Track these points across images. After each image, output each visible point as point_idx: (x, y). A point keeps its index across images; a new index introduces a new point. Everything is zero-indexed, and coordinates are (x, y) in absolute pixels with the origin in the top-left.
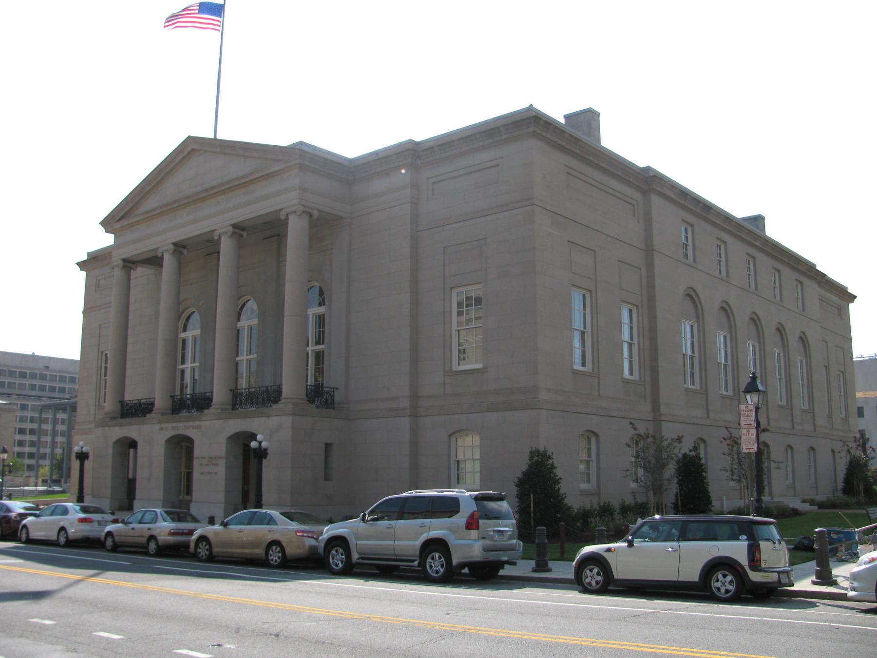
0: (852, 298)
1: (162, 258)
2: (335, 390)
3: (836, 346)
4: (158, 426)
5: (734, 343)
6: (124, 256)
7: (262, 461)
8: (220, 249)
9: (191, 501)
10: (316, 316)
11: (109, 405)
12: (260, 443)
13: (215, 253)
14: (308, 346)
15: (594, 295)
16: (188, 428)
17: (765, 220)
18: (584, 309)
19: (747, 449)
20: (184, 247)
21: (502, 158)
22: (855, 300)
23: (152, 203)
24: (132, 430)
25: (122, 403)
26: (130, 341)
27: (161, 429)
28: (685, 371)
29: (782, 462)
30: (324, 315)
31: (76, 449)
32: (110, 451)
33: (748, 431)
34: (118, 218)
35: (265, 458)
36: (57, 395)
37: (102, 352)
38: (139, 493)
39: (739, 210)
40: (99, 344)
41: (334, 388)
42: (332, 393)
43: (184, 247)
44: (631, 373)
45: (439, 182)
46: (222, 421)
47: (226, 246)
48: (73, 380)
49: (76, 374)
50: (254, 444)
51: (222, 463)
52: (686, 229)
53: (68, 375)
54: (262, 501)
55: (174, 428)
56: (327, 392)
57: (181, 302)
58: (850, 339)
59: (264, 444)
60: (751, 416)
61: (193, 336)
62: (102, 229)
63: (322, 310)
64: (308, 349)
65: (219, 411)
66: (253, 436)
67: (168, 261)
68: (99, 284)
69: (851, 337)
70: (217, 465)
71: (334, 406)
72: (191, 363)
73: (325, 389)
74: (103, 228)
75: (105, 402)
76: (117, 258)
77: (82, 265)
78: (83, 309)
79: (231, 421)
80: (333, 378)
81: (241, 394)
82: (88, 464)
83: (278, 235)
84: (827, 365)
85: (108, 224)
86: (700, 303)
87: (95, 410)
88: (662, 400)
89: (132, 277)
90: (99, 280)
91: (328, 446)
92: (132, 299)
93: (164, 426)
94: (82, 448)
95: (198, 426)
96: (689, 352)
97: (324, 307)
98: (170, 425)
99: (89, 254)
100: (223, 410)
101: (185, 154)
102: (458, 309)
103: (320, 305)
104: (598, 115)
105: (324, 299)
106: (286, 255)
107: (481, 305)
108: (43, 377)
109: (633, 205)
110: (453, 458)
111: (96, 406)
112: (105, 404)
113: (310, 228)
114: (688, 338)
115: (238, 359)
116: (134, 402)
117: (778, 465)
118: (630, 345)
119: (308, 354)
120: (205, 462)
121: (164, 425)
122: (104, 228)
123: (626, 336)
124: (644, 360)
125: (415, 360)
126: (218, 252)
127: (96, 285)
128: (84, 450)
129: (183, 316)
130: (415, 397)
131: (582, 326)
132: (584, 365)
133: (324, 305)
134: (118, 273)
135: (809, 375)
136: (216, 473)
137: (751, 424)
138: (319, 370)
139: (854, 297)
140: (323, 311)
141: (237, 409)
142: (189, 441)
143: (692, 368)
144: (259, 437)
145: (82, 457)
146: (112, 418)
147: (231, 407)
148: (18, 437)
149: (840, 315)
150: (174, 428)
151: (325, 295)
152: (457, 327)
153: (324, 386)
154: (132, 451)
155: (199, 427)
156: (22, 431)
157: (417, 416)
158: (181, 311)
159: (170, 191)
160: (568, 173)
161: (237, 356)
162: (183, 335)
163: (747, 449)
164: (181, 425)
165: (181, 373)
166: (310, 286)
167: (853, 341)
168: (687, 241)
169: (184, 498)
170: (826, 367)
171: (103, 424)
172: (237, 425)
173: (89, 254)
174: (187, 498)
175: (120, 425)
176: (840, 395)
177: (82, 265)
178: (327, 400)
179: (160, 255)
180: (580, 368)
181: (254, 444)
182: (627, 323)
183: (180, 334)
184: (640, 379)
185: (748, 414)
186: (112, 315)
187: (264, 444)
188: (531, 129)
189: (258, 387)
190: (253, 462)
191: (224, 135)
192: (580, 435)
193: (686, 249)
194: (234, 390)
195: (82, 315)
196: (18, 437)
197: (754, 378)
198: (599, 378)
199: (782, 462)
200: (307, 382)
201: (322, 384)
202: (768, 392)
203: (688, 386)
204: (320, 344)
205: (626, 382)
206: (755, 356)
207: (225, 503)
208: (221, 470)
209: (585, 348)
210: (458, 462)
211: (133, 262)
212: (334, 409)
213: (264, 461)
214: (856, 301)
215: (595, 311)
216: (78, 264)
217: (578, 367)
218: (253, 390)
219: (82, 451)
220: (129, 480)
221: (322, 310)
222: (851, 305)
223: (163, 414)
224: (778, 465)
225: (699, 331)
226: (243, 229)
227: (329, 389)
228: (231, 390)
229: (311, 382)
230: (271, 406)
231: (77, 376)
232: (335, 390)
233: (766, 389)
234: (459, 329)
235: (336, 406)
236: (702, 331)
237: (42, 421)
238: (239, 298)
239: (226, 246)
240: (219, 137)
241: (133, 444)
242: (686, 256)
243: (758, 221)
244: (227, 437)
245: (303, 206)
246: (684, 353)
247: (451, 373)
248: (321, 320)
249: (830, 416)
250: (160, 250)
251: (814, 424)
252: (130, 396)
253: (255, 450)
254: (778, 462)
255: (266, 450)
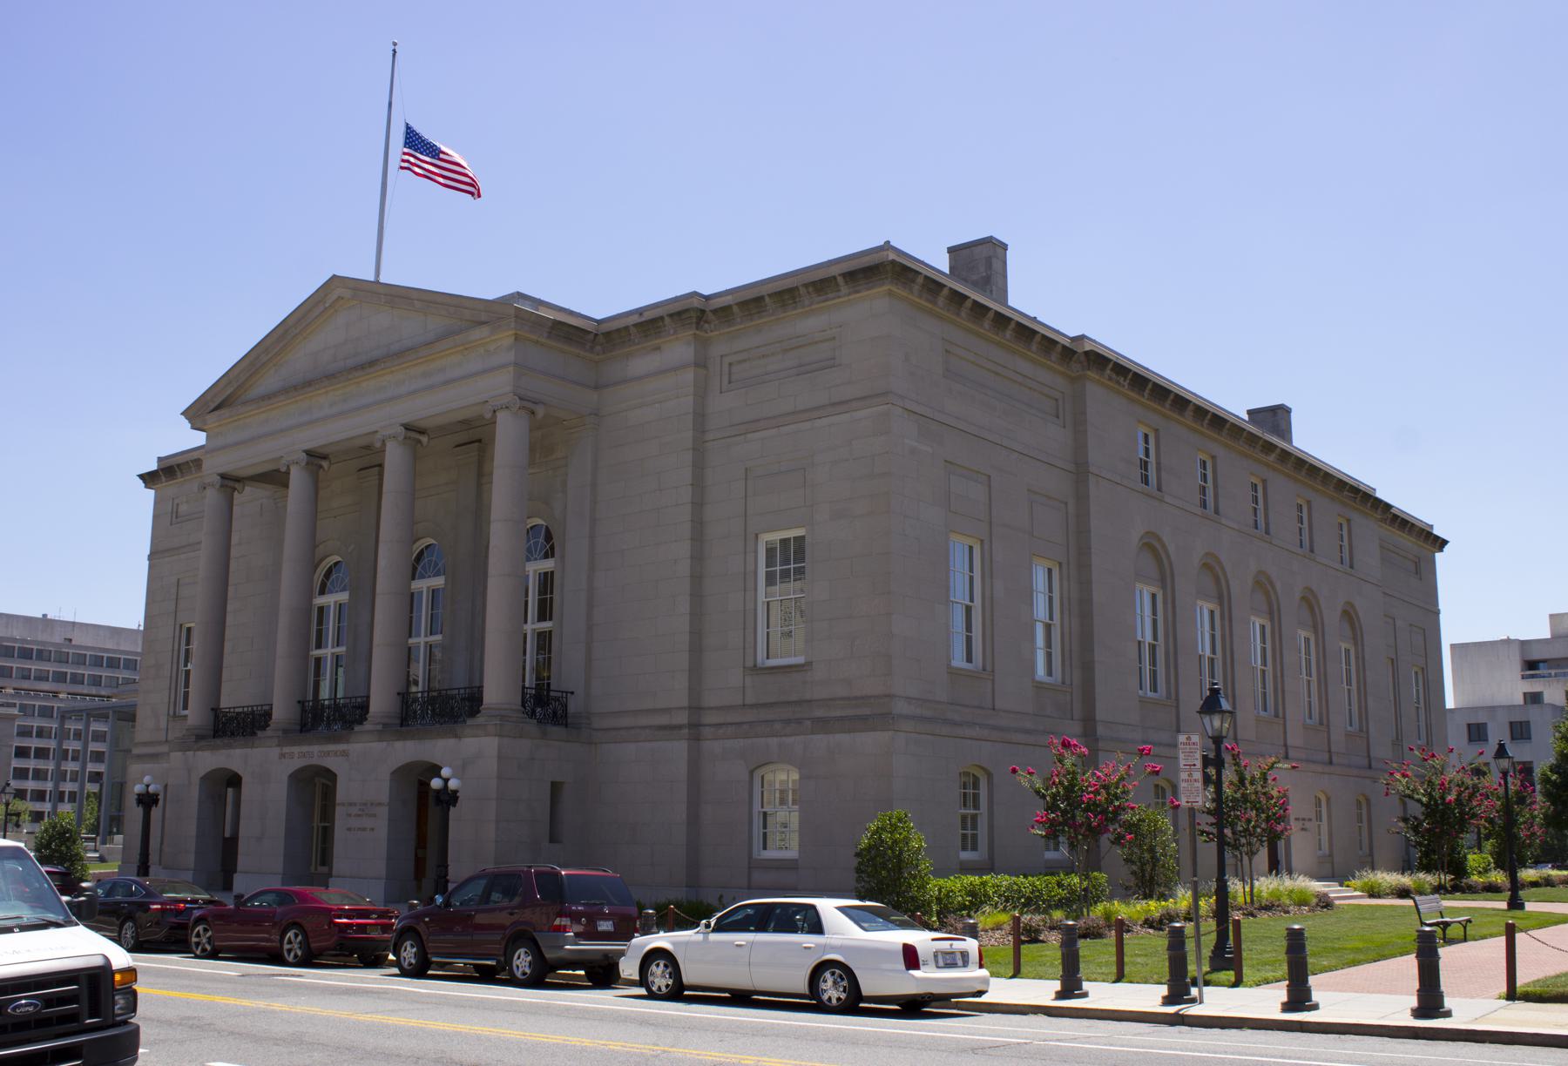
0: (1441, 544)
1: (287, 473)
2: (569, 695)
3: (1411, 625)
4: (275, 752)
5: (1227, 623)
6: (222, 470)
7: (449, 809)
8: (383, 459)
9: (330, 875)
10: (540, 574)
11: (195, 715)
12: (446, 781)
13: (375, 466)
14: (526, 622)
15: (986, 547)
16: (328, 754)
17: (1292, 414)
18: (971, 570)
19: (1188, 802)
20: (324, 457)
21: (841, 326)
22: (1446, 547)
23: (269, 381)
24: (233, 757)
25: (216, 711)
26: (230, 608)
27: (283, 756)
28: (1140, 668)
29: (1310, 820)
30: (552, 573)
31: (138, 788)
32: (195, 792)
33: (1190, 775)
34: (213, 406)
35: (455, 806)
36: (85, 689)
37: (181, 625)
38: (242, 861)
39: (1237, 403)
40: (176, 611)
41: (567, 693)
42: (564, 699)
43: (324, 457)
44: (1050, 673)
45: (740, 362)
46: (385, 744)
47: (395, 458)
48: (131, 665)
49: (136, 654)
50: (436, 783)
51: (384, 812)
52: (1146, 436)
53: (105, 655)
54: (447, 875)
55: (303, 755)
56: (556, 699)
57: (318, 546)
58: (1436, 613)
59: (453, 784)
60: (1195, 752)
61: (336, 602)
62: (186, 424)
63: (548, 565)
64: (525, 627)
65: (380, 727)
66: (435, 770)
67: (297, 478)
68: (177, 512)
69: (1439, 610)
70: (374, 815)
71: (567, 721)
72: (333, 647)
73: (552, 694)
74: (187, 421)
75: (185, 707)
76: (213, 467)
77: (149, 479)
78: (148, 553)
79: (399, 745)
80: (567, 675)
81: (415, 700)
82: (156, 812)
83: (479, 441)
84: (1394, 657)
85: (196, 414)
86: (1168, 556)
87: (744, 676)
88: (1100, 714)
89: (235, 502)
90: (178, 505)
91: (556, 788)
92: (235, 539)
93: (287, 751)
94: (148, 786)
95: (344, 751)
96: (1149, 638)
97: (553, 559)
98: (296, 750)
99: (160, 459)
100: (385, 725)
101: (327, 305)
102: (767, 567)
103: (546, 556)
104: (1004, 247)
105: (552, 548)
106: (491, 474)
107: (804, 562)
108: (63, 659)
109: (1057, 400)
110: (757, 807)
111: (168, 714)
112: (186, 712)
113: (531, 431)
114: (1146, 614)
115: (411, 641)
116: (237, 710)
117: (1303, 824)
118: (1048, 628)
119: (525, 635)
120: (354, 810)
121: (286, 750)
122: (190, 422)
123: (1041, 610)
124: (1071, 651)
125: (697, 648)
126: (381, 466)
127: (172, 512)
128: (151, 789)
129: (319, 570)
130: (696, 709)
131: (967, 597)
132: (969, 660)
133: (553, 556)
134: (212, 497)
135: (1323, 684)
136: (372, 829)
137: (1194, 765)
138: (544, 665)
139: (1444, 542)
140: (549, 566)
141: (408, 725)
142: (330, 776)
143: (1153, 662)
144: (445, 772)
145: (148, 801)
146: (200, 738)
147: (398, 721)
148: (17, 763)
149: (1417, 572)
150: (303, 755)
151: (554, 540)
152: (766, 597)
153: (552, 688)
154: (230, 790)
155: (345, 754)
156: (22, 753)
157: (699, 740)
158: (316, 562)
159: (300, 360)
160: (947, 351)
161: (410, 636)
162: (320, 601)
163: (1188, 802)
164: (316, 749)
165: (315, 662)
166: (530, 525)
167: (1442, 617)
168: (1147, 455)
169: (316, 869)
170: (1392, 660)
171: (184, 746)
172: (408, 750)
173: (160, 459)
174: (324, 869)
175: (214, 748)
176: (1418, 708)
177: (149, 479)
178: (555, 713)
179: (283, 469)
180: (965, 665)
181: (436, 783)
182: (1043, 591)
183: (316, 597)
184: (1063, 683)
185: (1190, 749)
186: (202, 562)
187: (453, 784)
188: (886, 288)
189: (443, 690)
190: (433, 811)
191: (392, 275)
192: (960, 774)
193: (1146, 470)
194: (403, 694)
195: (148, 562)
196: (17, 763)
197: (1215, 692)
198: (993, 680)
199: (1310, 820)
200: (524, 681)
201: (549, 684)
202: (1237, 714)
203: (1146, 694)
204: (545, 620)
205: (1039, 686)
206: (1264, 644)
207: (387, 879)
208: (380, 827)
209: (967, 636)
210: (765, 814)
211: (238, 480)
212: (566, 726)
213: (453, 812)
214: (1447, 548)
215: (989, 573)
216: (142, 477)
217: (959, 662)
218: (435, 694)
219: (148, 792)
220: (225, 839)
221: (548, 565)
222: (1438, 555)
223: (285, 731)
224: (1303, 824)
225: (1165, 603)
226: (422, 432)
227: (560, 694)
228: (399, 694)
229: (531, 679)
230: (464, 721)
231: (139, 658)
232: (569, 695)
233: (1234, 708)
234: (768, 600)
235: (569, 721)
236: (1171, 602)
237: (63, 735)
238: (415, 542)
239: (395, 458)
240: (382, 280)
241: (234, 781)
242: (1146, 480)
243: (1276, 417)
244: (392, 770)
245: (521, 399)
246: (1141, 639)
247: (756, 669)
248: (546, 581)
249: (1397, 741)
250: (283, 461)
251: (1369, 756)
252: (235, 697)
253: (438, 791)
254: (1304, 819)
255: (455, 792)
